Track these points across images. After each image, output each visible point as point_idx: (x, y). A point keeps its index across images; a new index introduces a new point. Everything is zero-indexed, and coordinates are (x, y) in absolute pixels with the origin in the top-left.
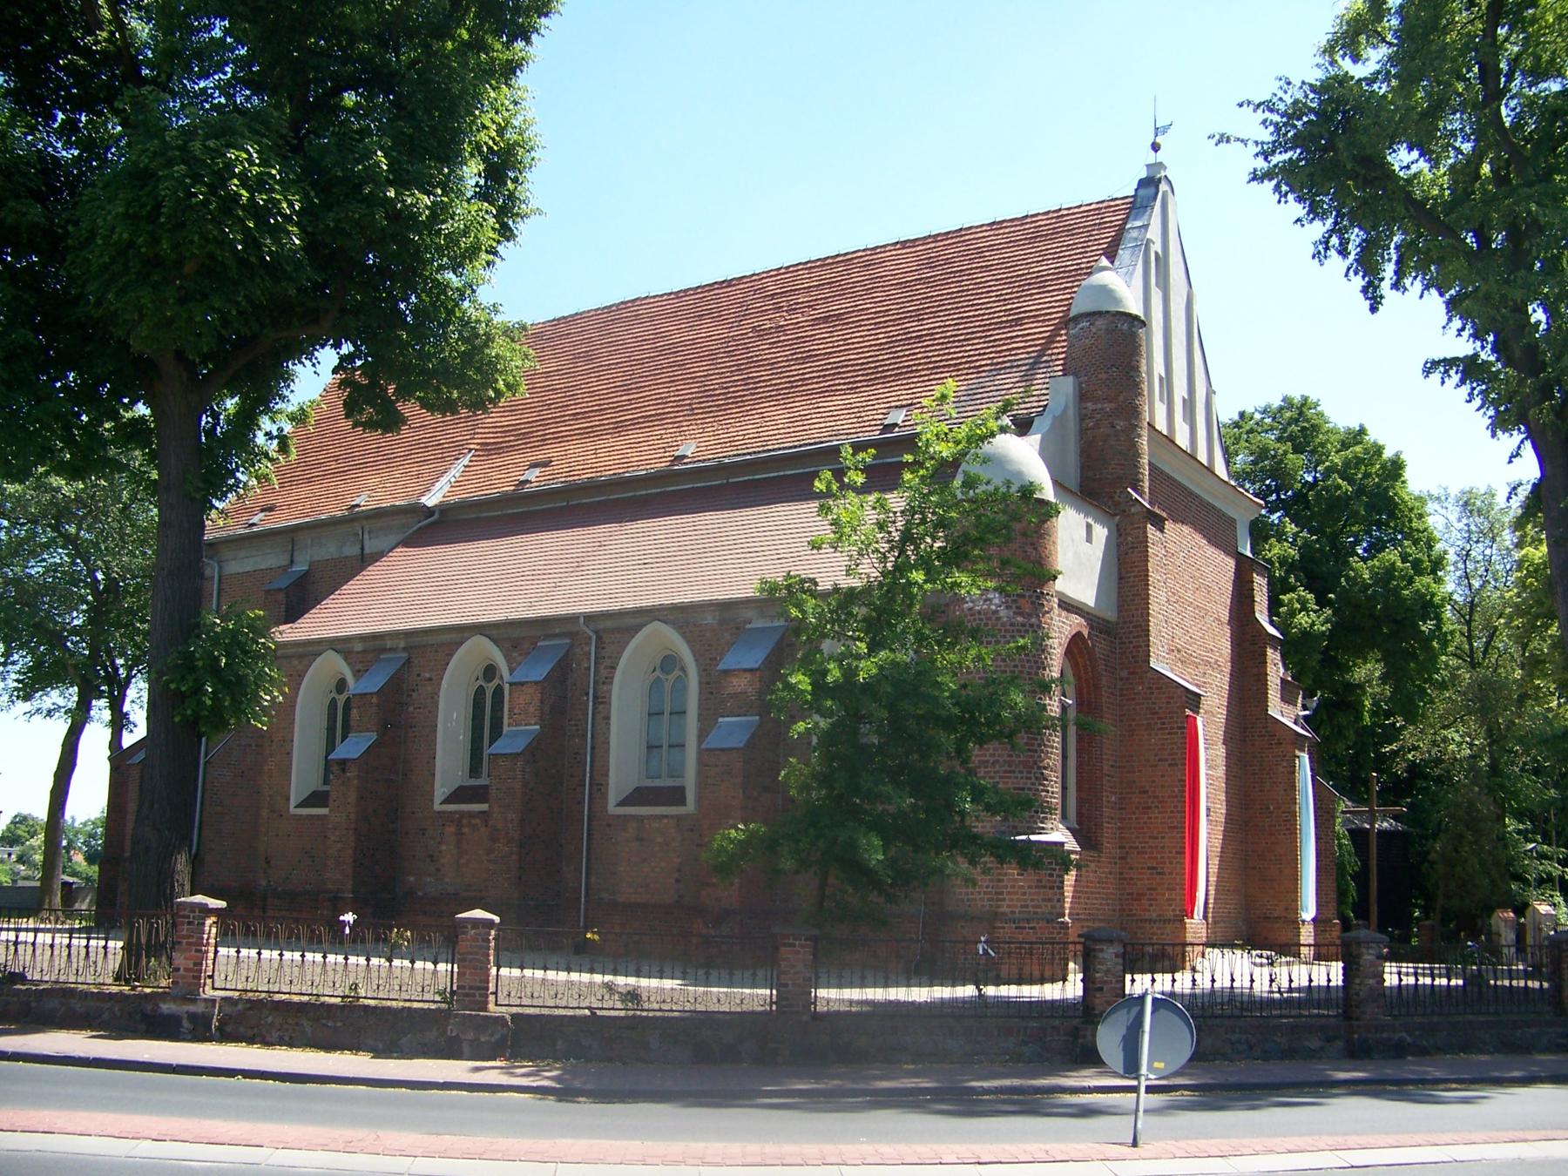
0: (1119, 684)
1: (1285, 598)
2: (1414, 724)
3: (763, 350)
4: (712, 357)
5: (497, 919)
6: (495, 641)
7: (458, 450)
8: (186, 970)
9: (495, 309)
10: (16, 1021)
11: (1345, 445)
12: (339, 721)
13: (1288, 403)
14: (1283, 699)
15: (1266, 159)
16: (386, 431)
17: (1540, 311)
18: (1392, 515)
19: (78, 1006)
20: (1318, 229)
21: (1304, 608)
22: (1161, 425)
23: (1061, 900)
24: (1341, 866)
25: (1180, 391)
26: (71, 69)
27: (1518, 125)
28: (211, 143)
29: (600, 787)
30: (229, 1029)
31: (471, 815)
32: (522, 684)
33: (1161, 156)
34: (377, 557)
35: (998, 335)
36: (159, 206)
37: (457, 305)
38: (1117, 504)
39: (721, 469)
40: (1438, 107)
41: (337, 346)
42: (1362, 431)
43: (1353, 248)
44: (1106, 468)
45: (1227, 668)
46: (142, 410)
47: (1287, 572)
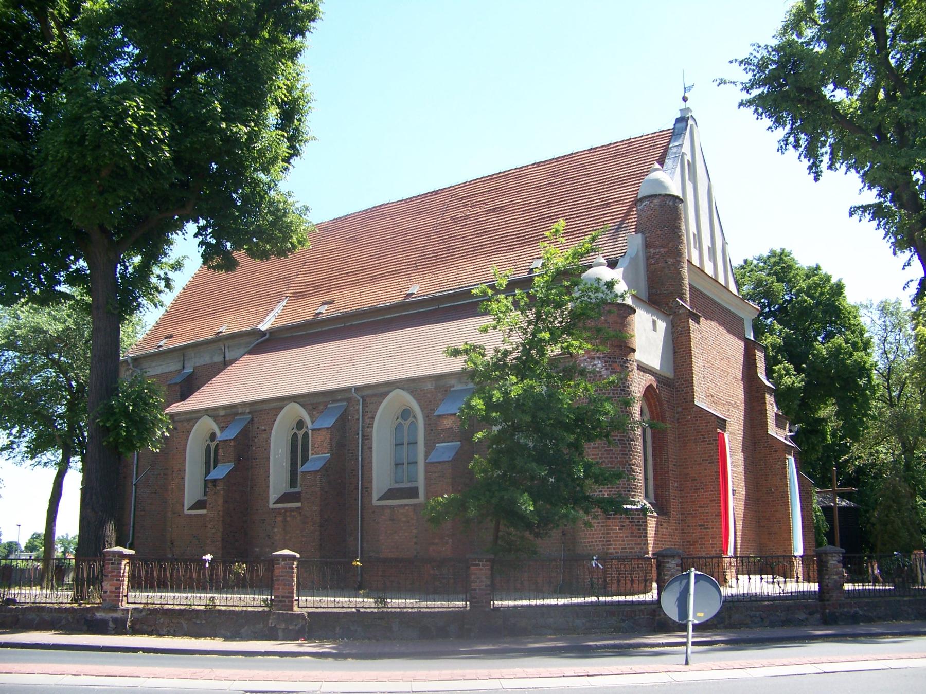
0: (677, 416)
1: (776, 368)
2: (858, 441)
3: (457, 229)
4: (428, 236)
5: (298, 555)
6: (302, 406)
7: (279, 297)
8: (111, 592)
9: (289, 194)
10: (10, 628)
11: (808, 277)
12: (211, 458)
13: (773, 254)
14: (777, 426)
15: (748, 92)
16: (227, 271)
17: (918, 173)
18: (838, 317)
19: (47, 617)
20: (781, 132)
21: (788, 373)
22: (696, 262)
23: (646, 544)
24: (817, 528)
25: (706, 242)
26: (37, 65)
27: (900, 64)
28: (114, 97)
29: (367, 490)
30: (137, 627)
31: (291, 510)
32: (319, 429)
33: (688, 104)
34: (232, 362)
35: (596, 213)
36: (84, 136)
37: (266, 193)
38: (671, 308)
39: (434, 300)
40: (849, 58)
41: (197, 221)
42: (818, 268)
43: (803, 143)
44: (664, 284)
45: (742, 407)
46: (82, 263)
47: (777, 353)
